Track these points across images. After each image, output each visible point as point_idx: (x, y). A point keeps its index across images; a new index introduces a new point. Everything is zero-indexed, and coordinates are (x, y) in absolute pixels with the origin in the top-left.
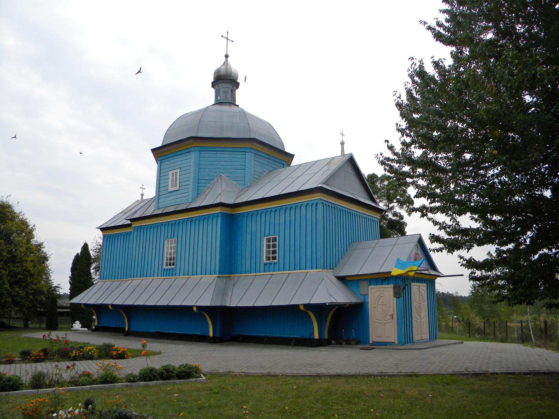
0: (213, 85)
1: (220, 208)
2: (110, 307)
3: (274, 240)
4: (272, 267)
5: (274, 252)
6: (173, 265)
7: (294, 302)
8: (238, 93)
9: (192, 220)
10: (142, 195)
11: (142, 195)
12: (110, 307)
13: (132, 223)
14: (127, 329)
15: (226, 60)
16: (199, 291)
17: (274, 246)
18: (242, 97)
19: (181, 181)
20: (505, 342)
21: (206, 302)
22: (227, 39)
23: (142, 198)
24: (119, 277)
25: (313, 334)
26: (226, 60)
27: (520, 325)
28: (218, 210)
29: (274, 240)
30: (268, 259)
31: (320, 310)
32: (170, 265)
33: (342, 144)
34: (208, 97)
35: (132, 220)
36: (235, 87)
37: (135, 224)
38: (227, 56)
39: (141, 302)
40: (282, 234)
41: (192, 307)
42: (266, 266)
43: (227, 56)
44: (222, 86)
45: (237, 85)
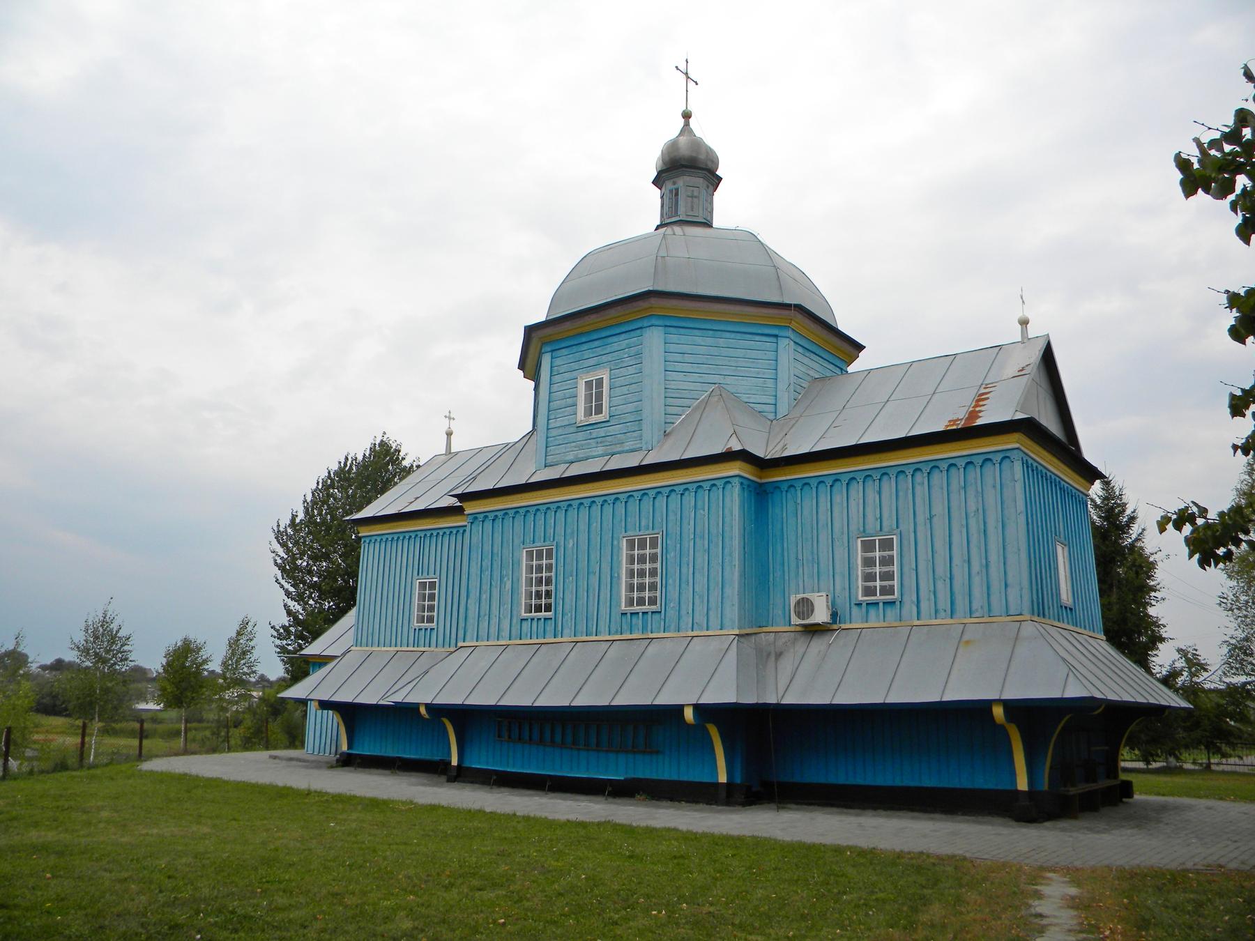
0: (657, 182)
1: (738, 464)
2: (423, 710)
3: (432, 585)
4: (638, 621)
5: (431, 608)
6: (548, 608)
7: (412, 699)
8: (720, 197)
9: (476, 518)
10: (1024, 323)
11: (1024, 323)
12: (423, 710)
13: (465, 505)
14: (454, 762)
15: (687, 124)
16: (697, 670)
17: (432, 597)
18: (731, 207)
19: (616, 401)
20: (222, 751)
21: (723, 692)
22: (688, 77)
23: (1024, 332)
24: (405, 641)
25: (1014, 781)
26: (687, 124)
27: (137, 725)
28: (734, 469)
29: (432, 585)
30: (630, 602)
31: (1032, 716)
32: (641, 601)
33: (449, 434)
34: (642, 210)
35: (463, 497)
36: (711, 188)
37: (471, 508)
38: (687, 116)
39: (548, 700)
40: (907, 526)
41: (679, 709)
42: (524, 623)
43: (687, 116)
44: (683, 182)
45: (714, 181)
